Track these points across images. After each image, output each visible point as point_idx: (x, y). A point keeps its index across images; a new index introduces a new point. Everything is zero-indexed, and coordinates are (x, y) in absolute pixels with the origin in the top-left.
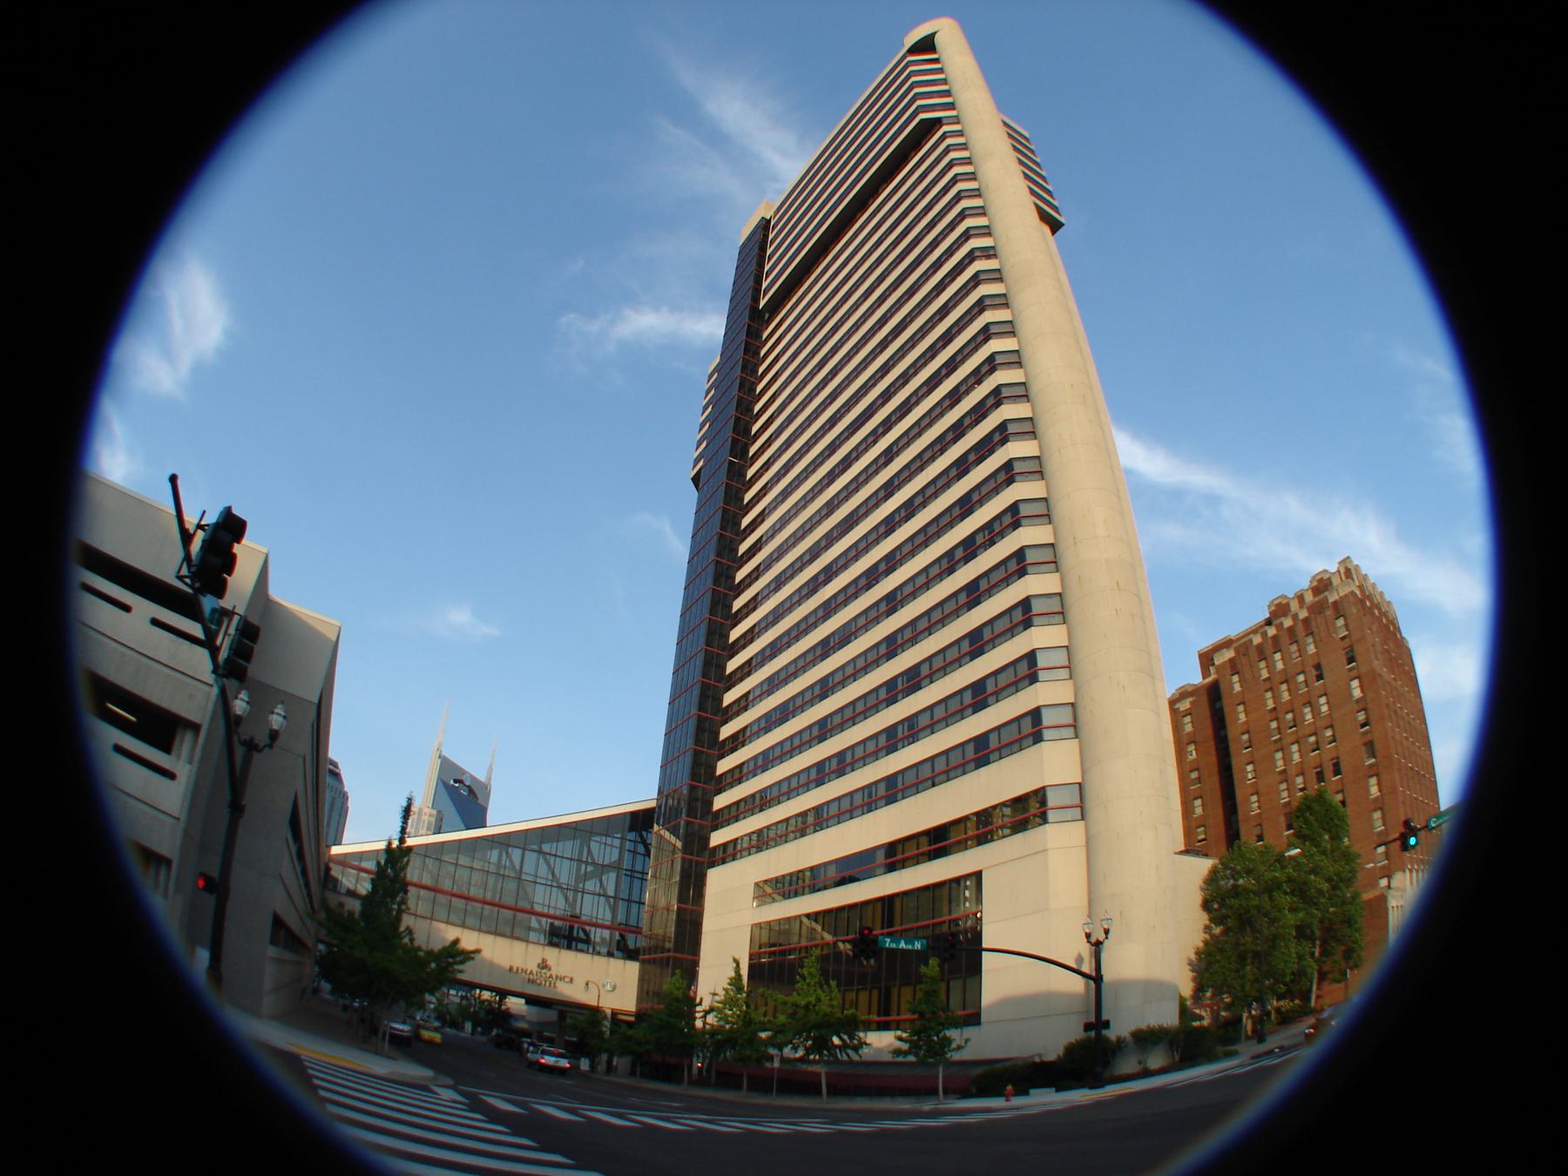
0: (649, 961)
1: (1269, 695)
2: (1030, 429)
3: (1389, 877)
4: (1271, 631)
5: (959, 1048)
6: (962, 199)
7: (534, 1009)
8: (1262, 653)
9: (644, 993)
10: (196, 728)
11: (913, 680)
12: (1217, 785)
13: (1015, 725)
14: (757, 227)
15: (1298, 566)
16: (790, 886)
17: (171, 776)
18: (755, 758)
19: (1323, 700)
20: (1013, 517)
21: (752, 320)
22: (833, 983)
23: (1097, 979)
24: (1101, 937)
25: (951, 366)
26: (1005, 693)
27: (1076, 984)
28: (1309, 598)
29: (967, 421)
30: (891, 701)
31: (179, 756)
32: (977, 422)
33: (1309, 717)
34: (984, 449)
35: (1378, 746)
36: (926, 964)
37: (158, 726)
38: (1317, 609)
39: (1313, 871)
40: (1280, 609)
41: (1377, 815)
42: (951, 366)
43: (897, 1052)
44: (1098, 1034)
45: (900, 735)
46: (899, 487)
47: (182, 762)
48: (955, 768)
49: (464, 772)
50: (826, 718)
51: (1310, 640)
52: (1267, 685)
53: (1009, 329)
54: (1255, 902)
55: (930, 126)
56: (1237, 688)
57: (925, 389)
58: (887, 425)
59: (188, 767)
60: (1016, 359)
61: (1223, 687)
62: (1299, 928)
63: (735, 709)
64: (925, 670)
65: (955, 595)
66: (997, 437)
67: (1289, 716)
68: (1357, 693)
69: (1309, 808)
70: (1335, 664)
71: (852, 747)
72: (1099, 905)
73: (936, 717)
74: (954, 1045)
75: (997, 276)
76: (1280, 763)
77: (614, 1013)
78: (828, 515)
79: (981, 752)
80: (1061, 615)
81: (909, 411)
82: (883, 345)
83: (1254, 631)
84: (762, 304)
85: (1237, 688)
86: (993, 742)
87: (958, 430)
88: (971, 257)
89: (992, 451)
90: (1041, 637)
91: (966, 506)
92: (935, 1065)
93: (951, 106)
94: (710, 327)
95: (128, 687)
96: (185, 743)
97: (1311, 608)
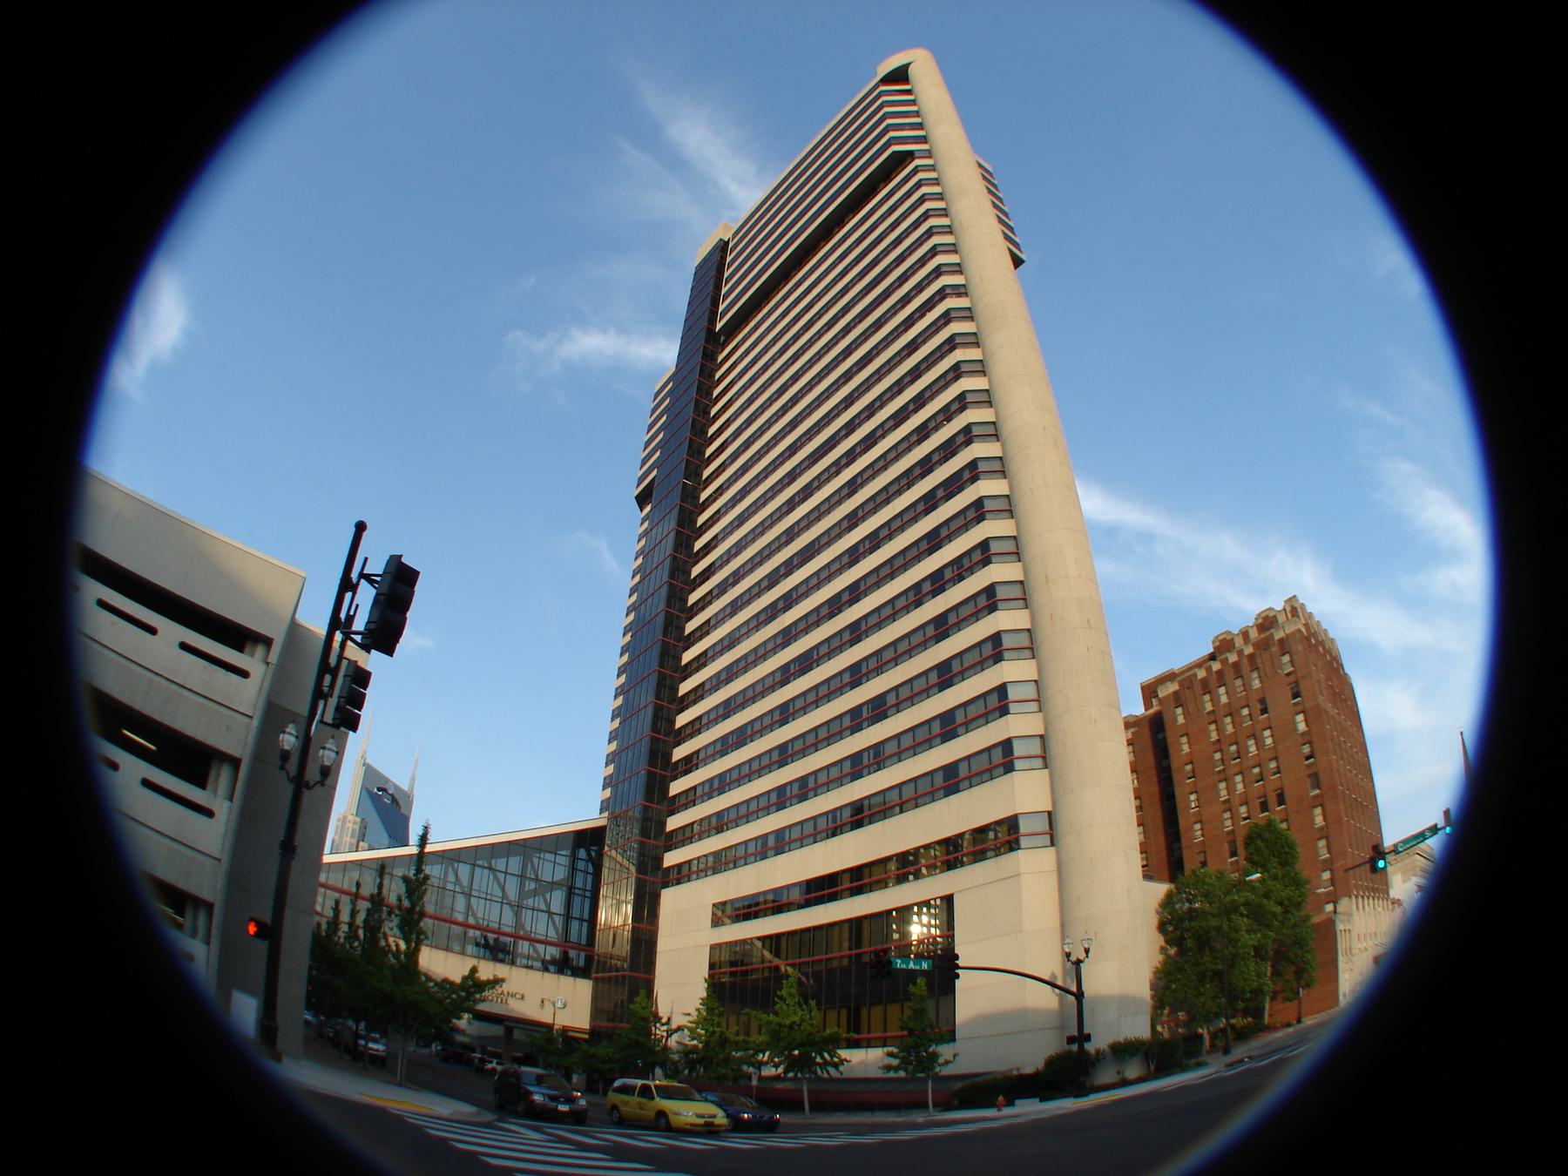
0: (603, 979)
1: (1213, 727)
2: (1000, 468)
3: (1335, 903)
4: (1216, 666)
5: (947, 1062)
6: (933, 236)
7: (476, 1023)
8: (1206, 687)
9: (596, 1011)
10: (235, 763)
11: (879, 709)
12: (1159, 814)
13: (985, 755)
14: (715, 249)
15: (1242, 609)
16: (749, 909)
17: (209, 813)
18: (711, 780)
19: (1267, 733)
20: (983, 554)
21: (706, 342)
22: (813, 1003)
23: (1079, 995)
24: (1082, 955)
25: (920, 401)
26: (975, 724)
27: (1046, 999)
28: (1254, 634)
29: (936, 458)
30: (856, 728)
31: (215, 792)
32: (945, 459)
33: (1253, 749)
34: (953, 486)
35: (1322, 777)
36: (915, 984)
37: (188, 758)
38: (1263, 645)
39: (1267, 896)
40: (1224, 645)
41: (1322, 843)
42: (920, 401)
43: (888, 1068)
44: (1081, 1047)
45: (865, 762)
46: (864, 519)
47: (219, 797)
48: (923, 795)
49: (387, 781)
50: (786, 743)
51: (1255, 675)
52: (1212, 717)
53: (981, 369)
54: (1214, 922)
55: (902, 159)
56: (1181, 720)
57: (891, 423)
58: (851, 456)
59: (227, 804)
60: (986, 399)
61: (1166, 718)
62: (1256, 948)
63: (689, 731)
64: (891, 700)
65: (923, 627)
66: (967, 475)
67: (1233, 748)
68: (1302, 727)
69: (1260, 836)
70: (1280, 700)
71: (815, 773)
72: (1056, 927)
73: (903, 746)
74: (941, 1060)
75: (968, 314)
76: (1223, 792)
77: (565, 1030)
78: (787, 543)
79: (951, 780)
80: (1032, 650)
81: (874, 444)
82: (848, 376)
83: (1199, 665)
84: (719, 326)
85: (1181, 720)
86: (963, 771)
87: (926, 466)
88: (942, 294)
89: (960, 489)
90: (1012, 670)
91: (934, 541)
92: (924, 1080)
93: (924, 140)
94: (662, 353)
95: (156, 717)
96: (223, 776)
97: (1256, 645)
